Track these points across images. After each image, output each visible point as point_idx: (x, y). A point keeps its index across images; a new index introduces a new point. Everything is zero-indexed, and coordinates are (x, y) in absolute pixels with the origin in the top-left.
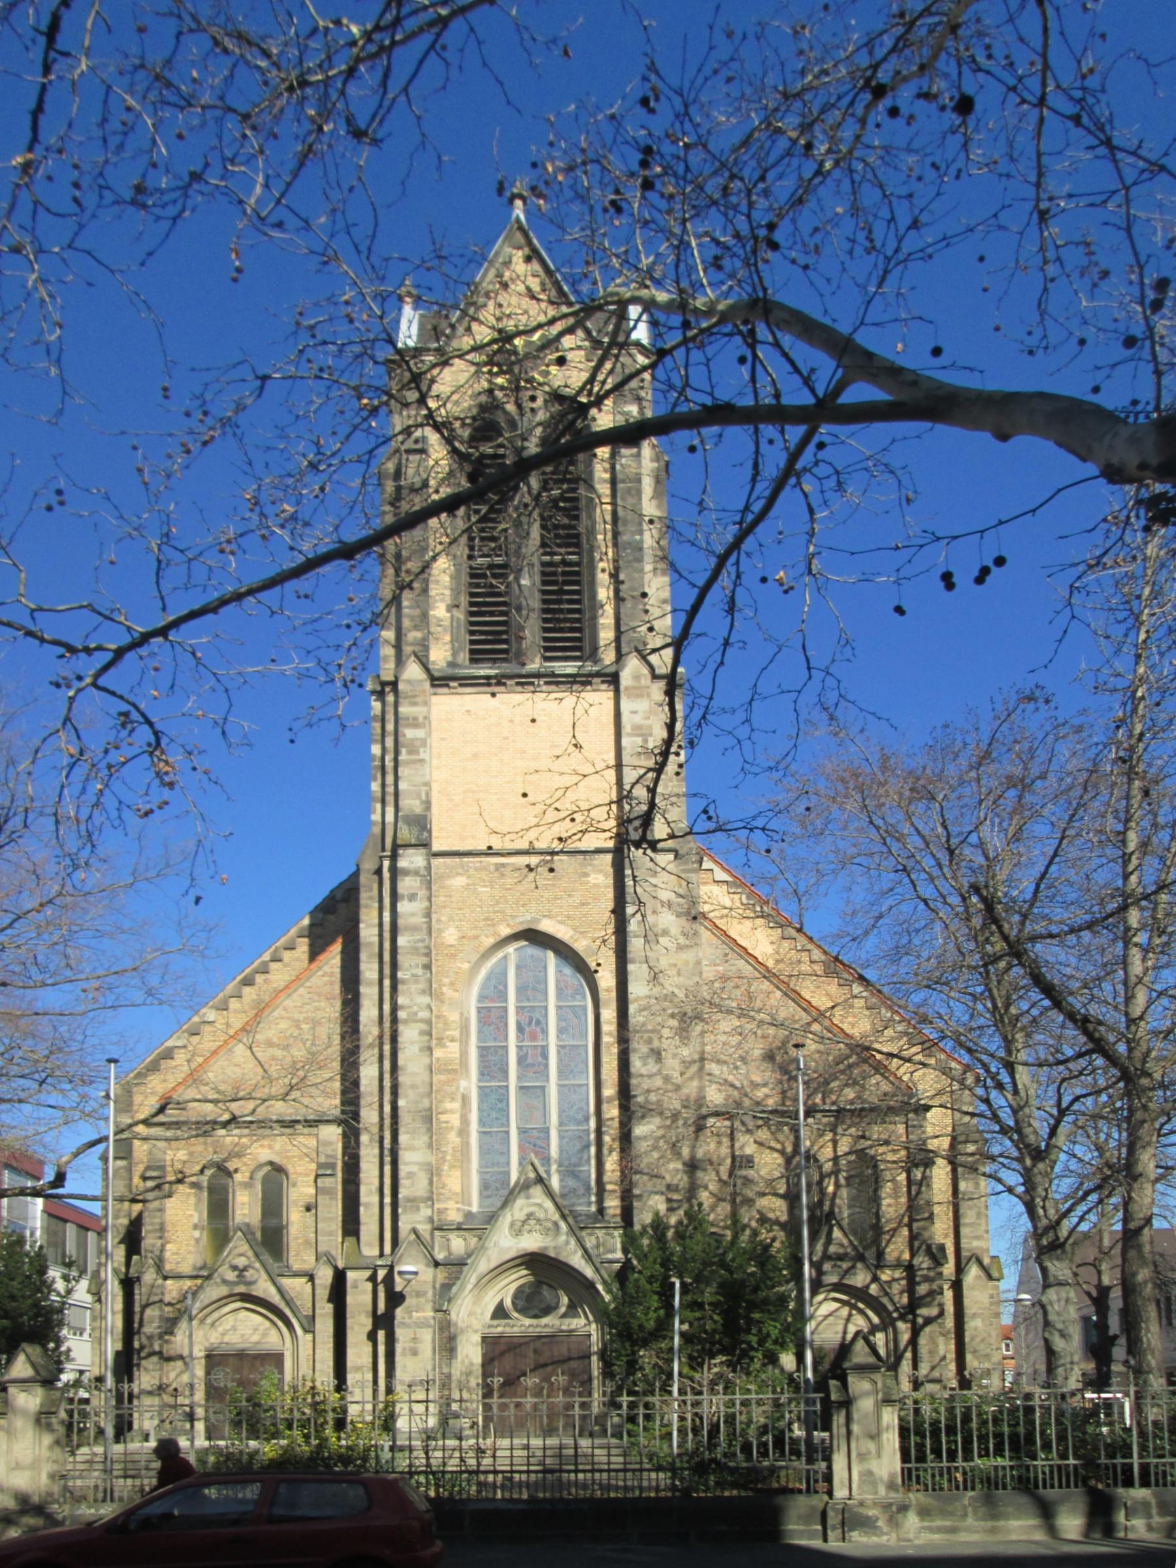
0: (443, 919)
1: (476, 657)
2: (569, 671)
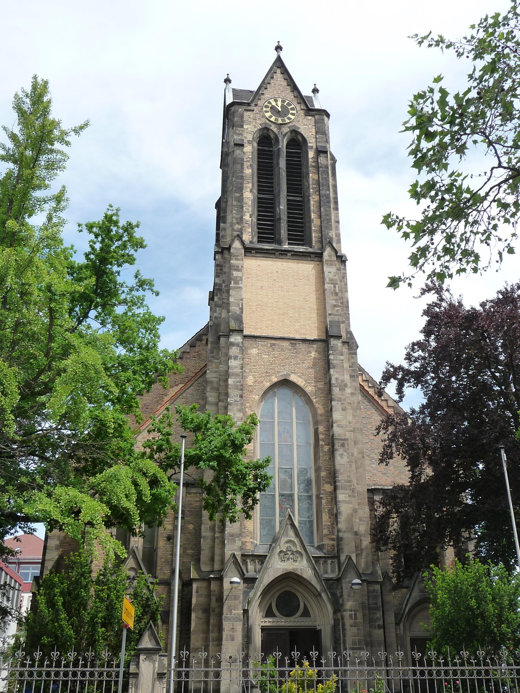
0: (247, 371)
1: (261, 240)
2: (301, 250)
